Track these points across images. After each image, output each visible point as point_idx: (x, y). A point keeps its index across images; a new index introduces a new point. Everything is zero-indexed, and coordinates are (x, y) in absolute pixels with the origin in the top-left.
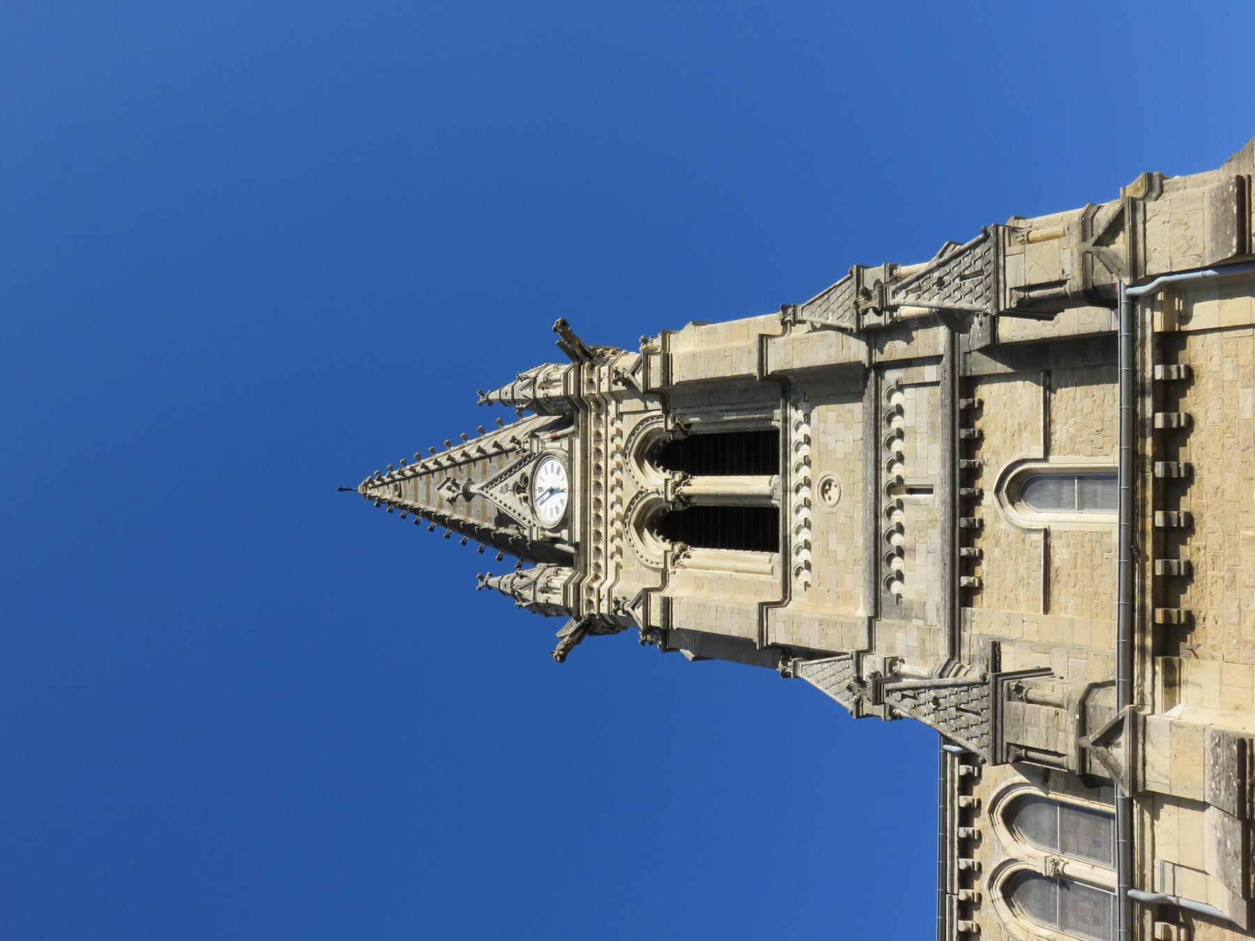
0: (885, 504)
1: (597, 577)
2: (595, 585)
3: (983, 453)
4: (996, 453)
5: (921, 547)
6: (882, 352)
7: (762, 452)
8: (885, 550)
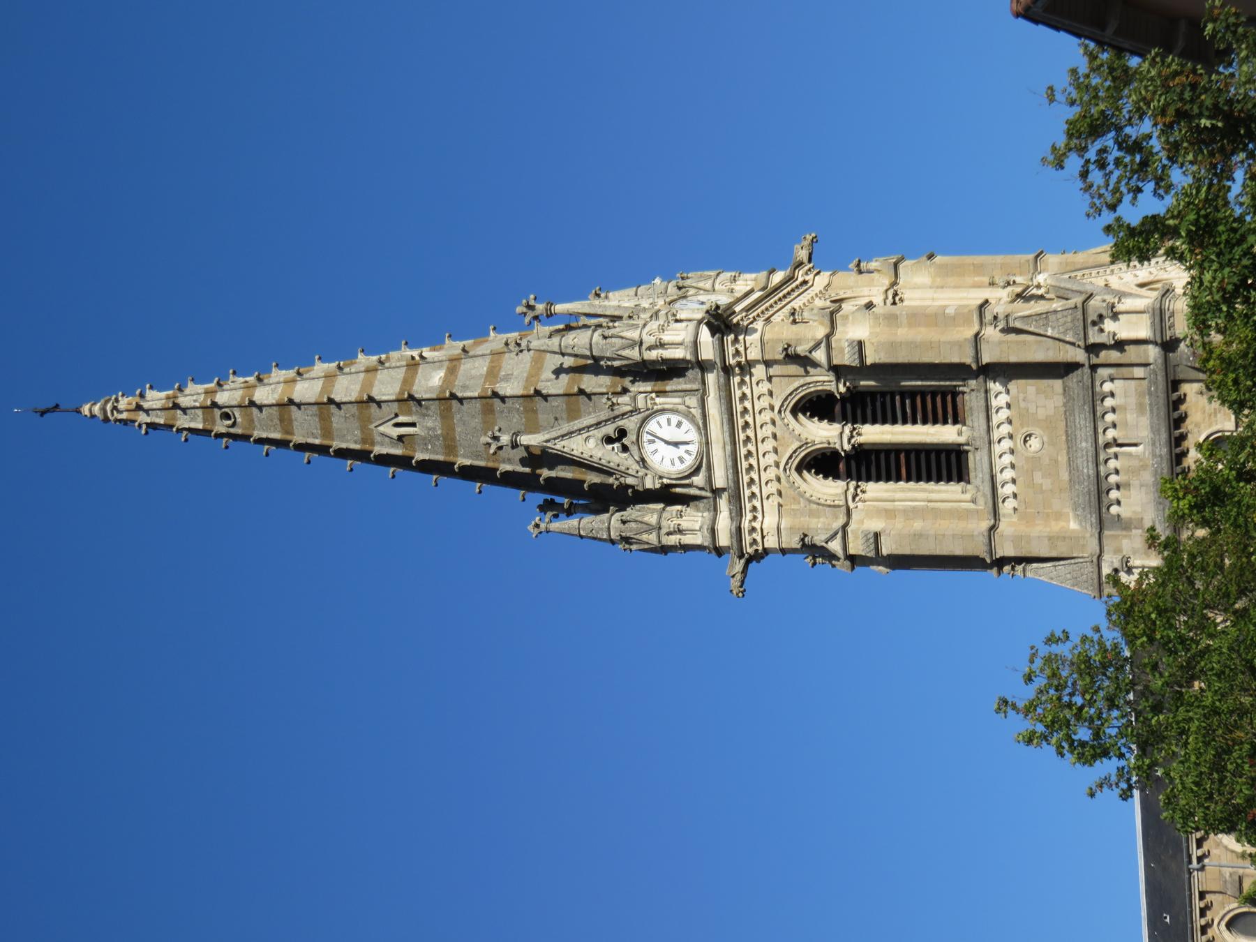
0: (1102, 457)
1: (755, 518)
2: (757, 525)
3: (1188, 425)
4: (1198, 425)
5: (1135, 482)
6: (1097, 356)
7: (944, 407)
8: (1104, 487)
